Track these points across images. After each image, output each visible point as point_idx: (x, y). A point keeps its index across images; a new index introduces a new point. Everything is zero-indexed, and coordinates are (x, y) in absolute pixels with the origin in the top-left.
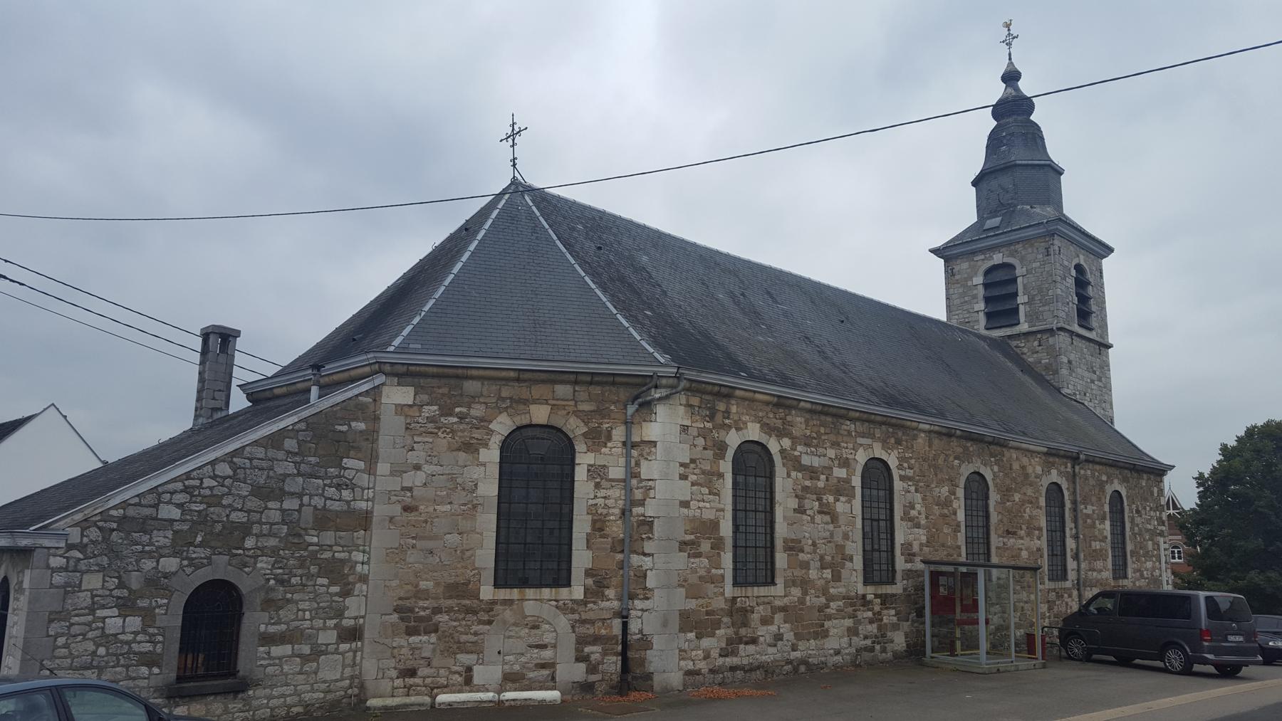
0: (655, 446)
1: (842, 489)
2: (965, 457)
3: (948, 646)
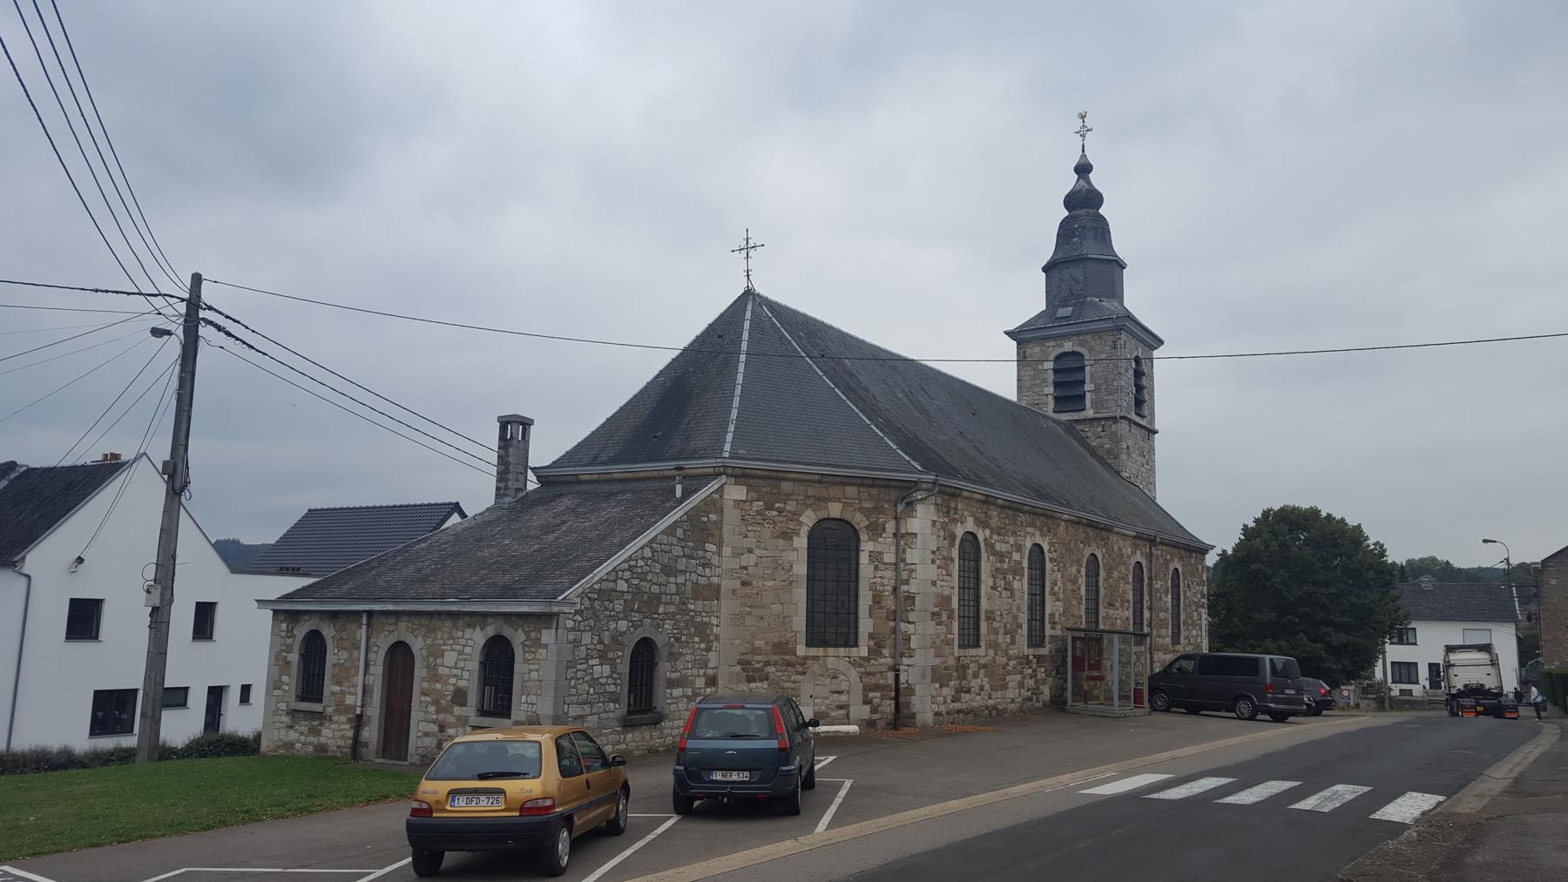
0: (916, 537)
1: (1016, 570)
2: (1086, 542)
3: (1085, 697)
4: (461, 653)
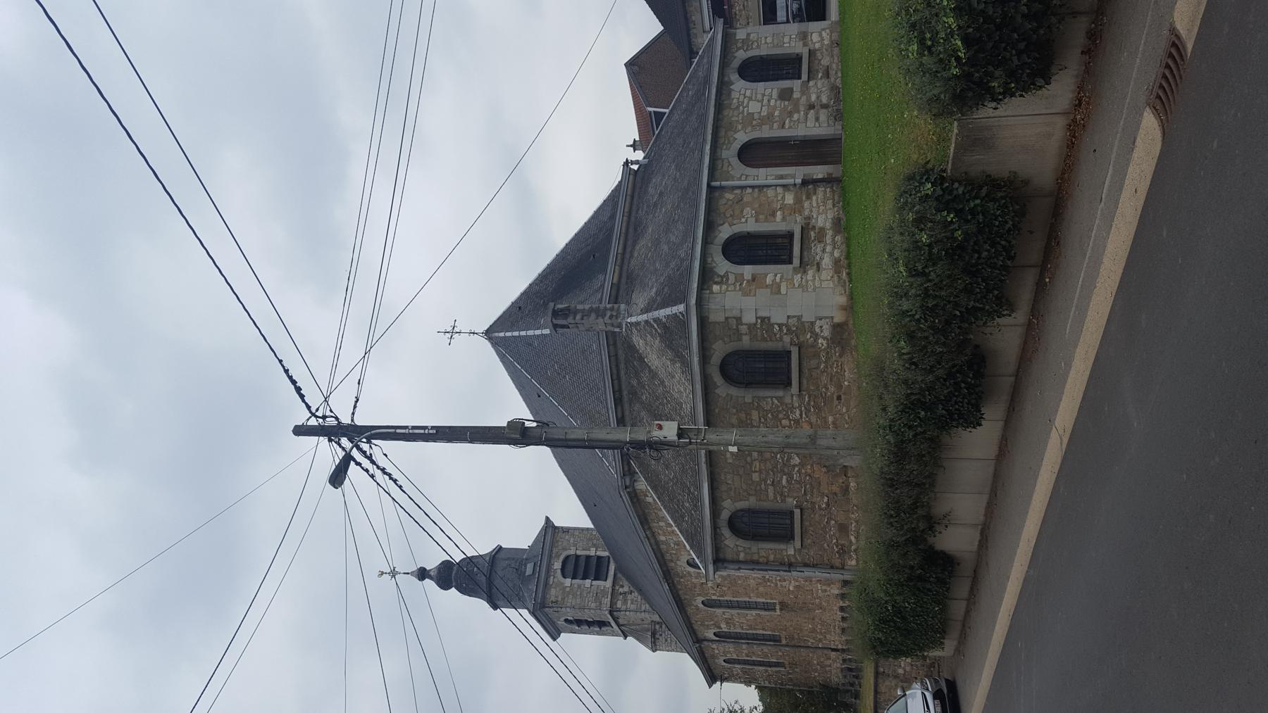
4: (750, 99)
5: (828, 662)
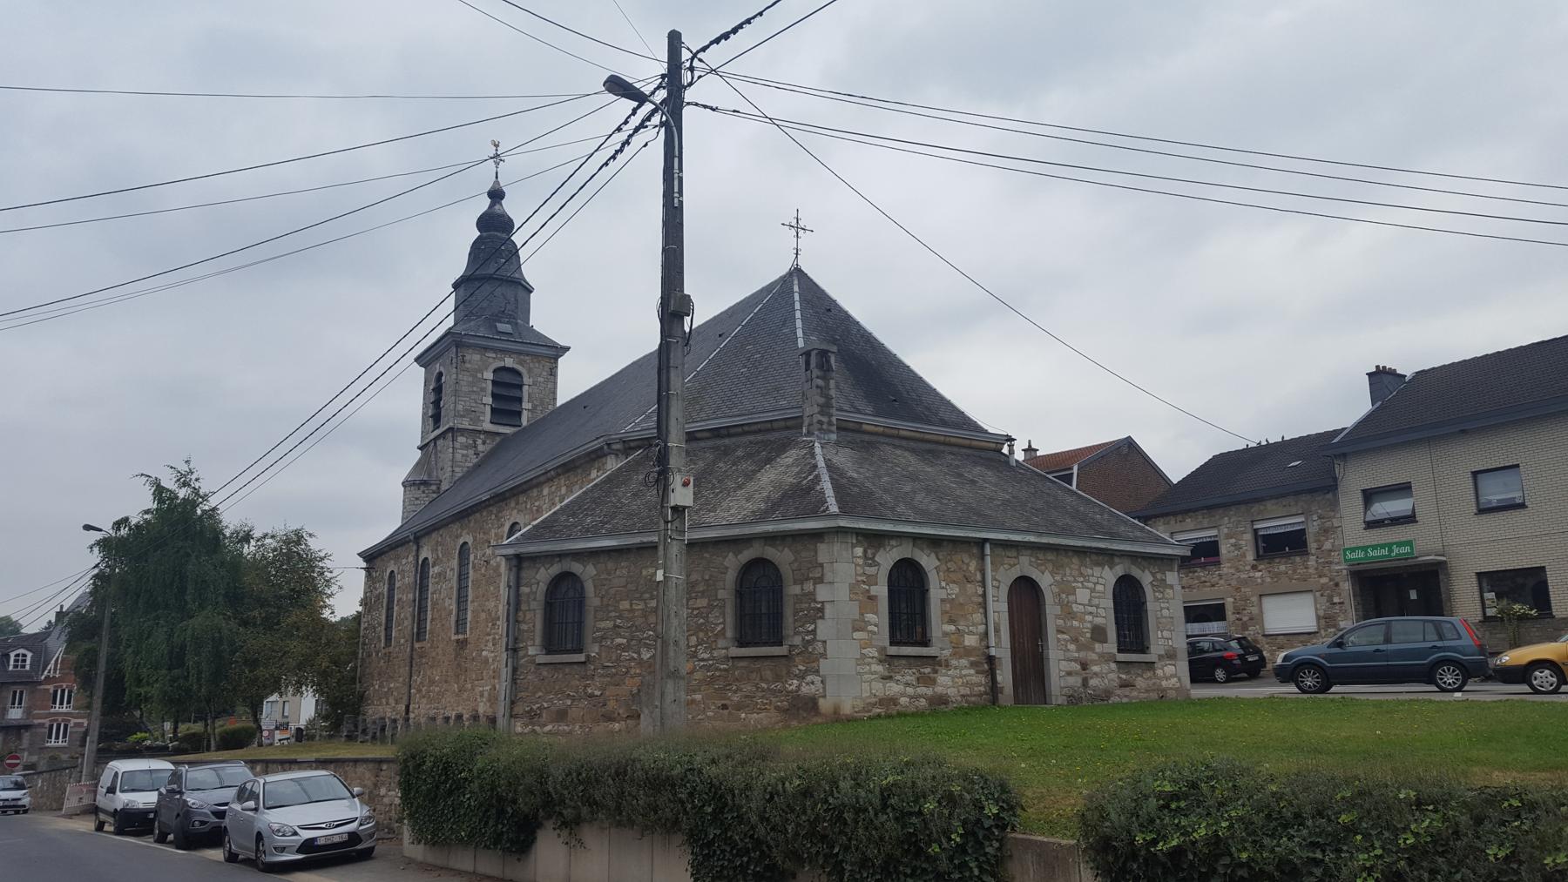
4: (1093, 590)
5: (392, 701)
